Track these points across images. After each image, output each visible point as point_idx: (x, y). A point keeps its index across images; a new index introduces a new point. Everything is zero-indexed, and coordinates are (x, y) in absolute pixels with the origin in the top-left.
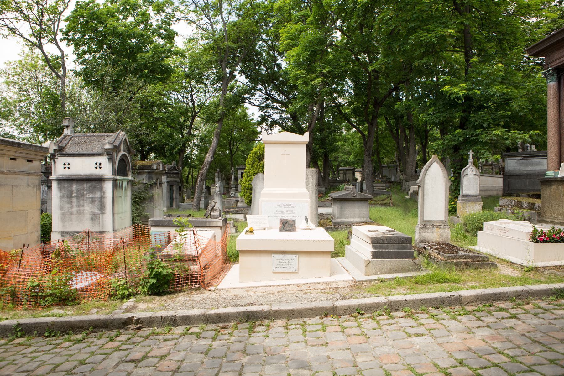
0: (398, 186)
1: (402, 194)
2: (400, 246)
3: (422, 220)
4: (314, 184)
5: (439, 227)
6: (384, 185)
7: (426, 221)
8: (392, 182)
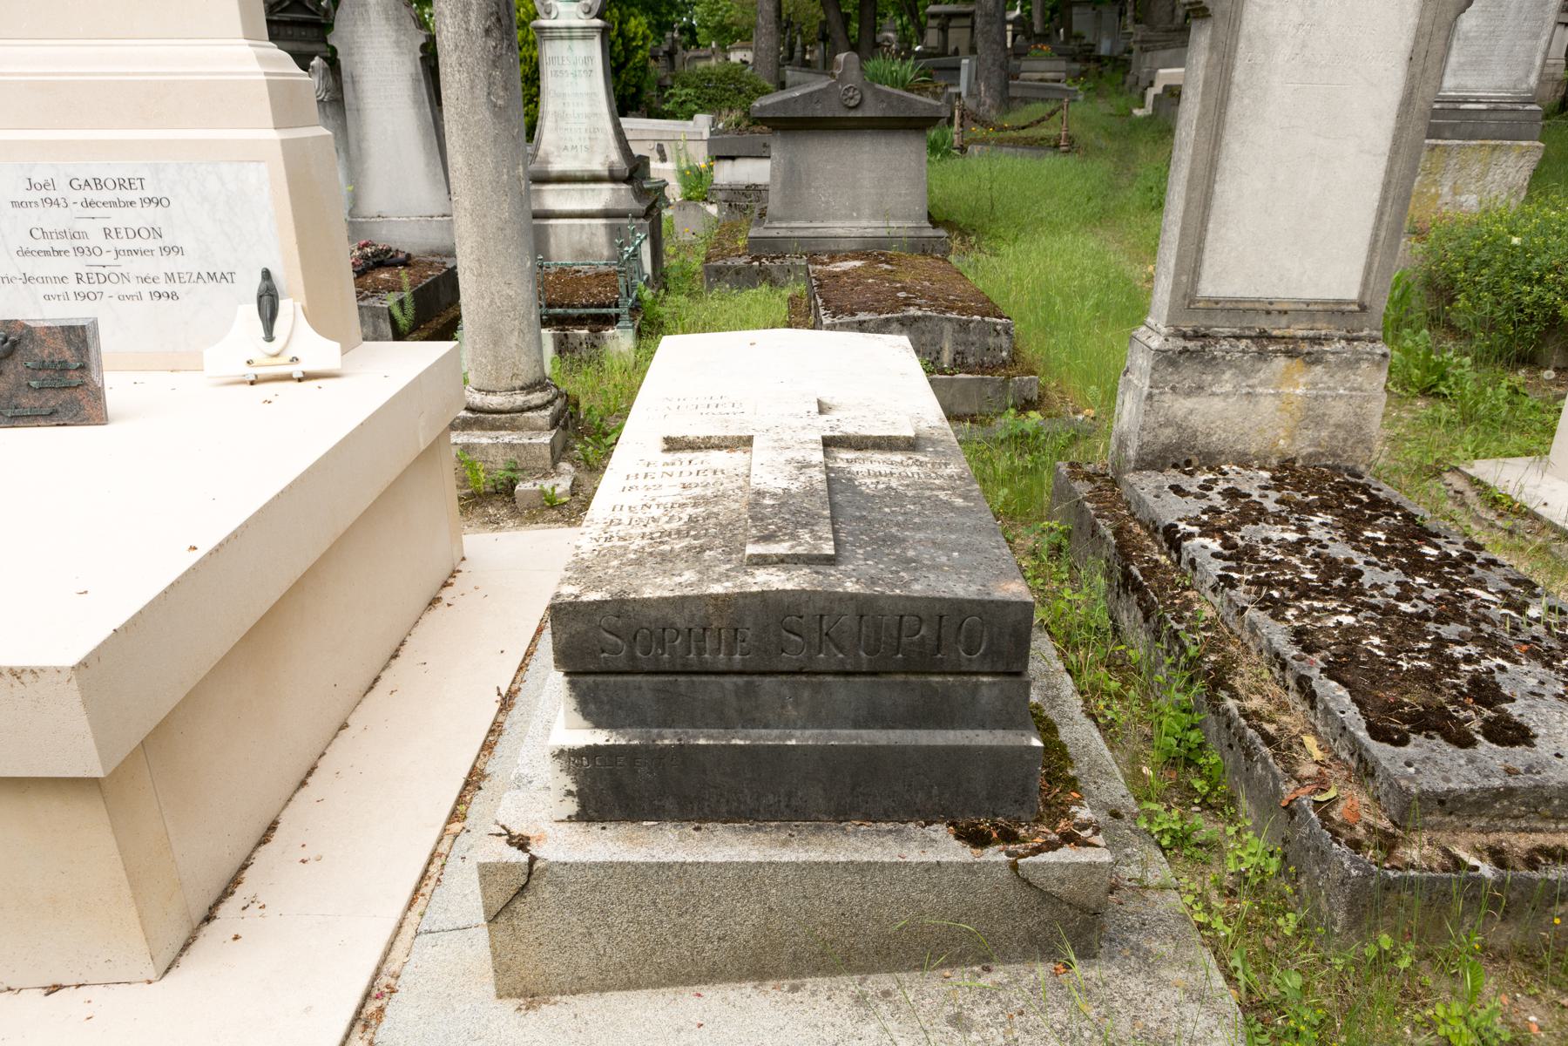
0: (1109, 71)
1: (1122, 101)
2: (892, 691)
3: (1187, 299)
4: (476, 24)
5: (1303, 351)
6: (1063, 65)
7: (1217, 306)
8: (1099, 59)
